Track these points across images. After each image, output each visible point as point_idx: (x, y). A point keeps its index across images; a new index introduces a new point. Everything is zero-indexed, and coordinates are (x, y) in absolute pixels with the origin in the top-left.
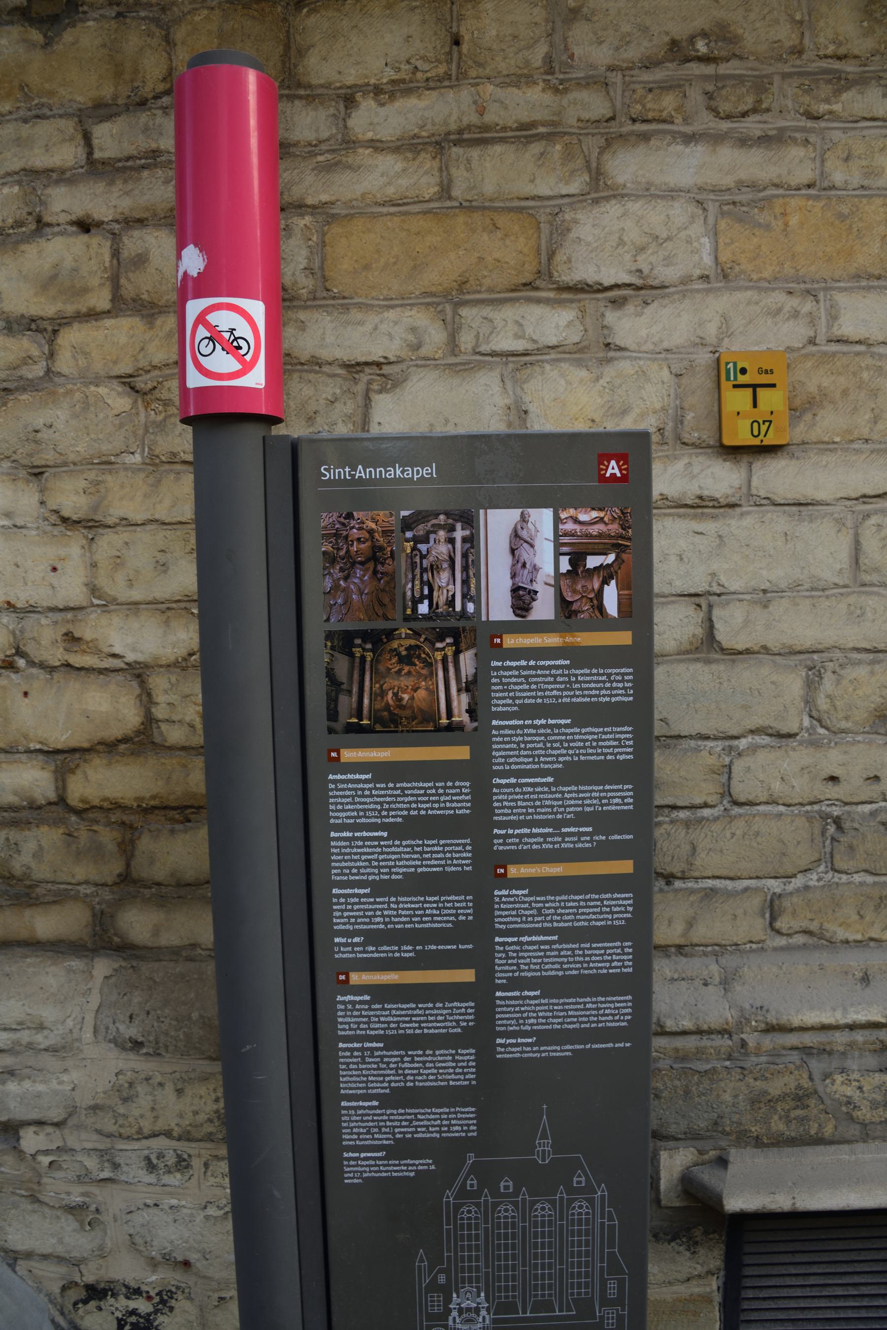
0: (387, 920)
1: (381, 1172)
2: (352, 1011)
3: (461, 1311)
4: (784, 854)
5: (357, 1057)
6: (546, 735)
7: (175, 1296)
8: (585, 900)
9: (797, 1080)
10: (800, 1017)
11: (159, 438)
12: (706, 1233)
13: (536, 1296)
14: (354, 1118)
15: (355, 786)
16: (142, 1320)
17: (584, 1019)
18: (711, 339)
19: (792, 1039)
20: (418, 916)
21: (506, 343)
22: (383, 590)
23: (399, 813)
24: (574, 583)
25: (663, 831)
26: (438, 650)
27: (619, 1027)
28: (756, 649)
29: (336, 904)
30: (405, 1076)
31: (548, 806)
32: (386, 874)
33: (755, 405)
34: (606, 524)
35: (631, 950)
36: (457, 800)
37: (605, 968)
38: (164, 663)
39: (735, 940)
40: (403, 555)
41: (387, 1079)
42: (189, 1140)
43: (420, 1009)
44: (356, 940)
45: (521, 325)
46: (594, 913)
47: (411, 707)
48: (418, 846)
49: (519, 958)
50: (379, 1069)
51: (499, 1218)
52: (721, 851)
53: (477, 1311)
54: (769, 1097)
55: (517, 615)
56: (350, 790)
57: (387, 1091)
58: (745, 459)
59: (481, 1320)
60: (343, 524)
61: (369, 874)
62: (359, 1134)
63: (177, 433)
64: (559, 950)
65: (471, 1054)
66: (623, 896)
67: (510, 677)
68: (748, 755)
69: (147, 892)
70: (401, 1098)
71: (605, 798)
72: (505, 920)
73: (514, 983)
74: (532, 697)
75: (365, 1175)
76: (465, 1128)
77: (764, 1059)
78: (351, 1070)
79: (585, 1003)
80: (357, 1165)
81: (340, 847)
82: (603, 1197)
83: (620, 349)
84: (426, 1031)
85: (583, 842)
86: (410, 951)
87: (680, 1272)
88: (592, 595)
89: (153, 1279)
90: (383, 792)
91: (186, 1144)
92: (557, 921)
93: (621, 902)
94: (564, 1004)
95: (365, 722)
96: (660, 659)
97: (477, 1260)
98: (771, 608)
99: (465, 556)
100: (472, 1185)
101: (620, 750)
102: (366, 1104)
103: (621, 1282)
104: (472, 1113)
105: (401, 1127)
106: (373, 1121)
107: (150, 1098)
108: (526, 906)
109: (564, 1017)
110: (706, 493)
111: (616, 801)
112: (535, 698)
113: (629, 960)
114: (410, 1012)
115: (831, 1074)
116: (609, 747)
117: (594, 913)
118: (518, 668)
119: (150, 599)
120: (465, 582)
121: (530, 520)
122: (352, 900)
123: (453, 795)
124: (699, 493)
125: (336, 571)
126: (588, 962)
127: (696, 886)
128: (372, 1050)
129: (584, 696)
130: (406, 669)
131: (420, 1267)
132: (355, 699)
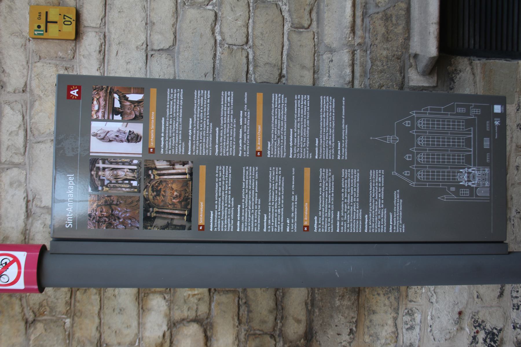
0: (279, 207)
1: (399, 215)
2: (322, 225)
3: (469, 181)
4: (272, 21)
5: (344, 224)
6: (197, 130)
7: (476, 319)
8: (275, 116)
9: (378, 20)
10: (348, 17)
11: (58, 310)
12: (451, 65)
13: (463, 146)
14: (373, 226)
15: (216, 219)
16: (489, 336)
17: (330, 118)
18: (23, 41)
19: (359, 21)
20: (278, 193)
21: (20, 140)
22: (125, 202)
23: (229, 199)
24: (126, 113)
25: (258, 78)
26: (154, 178)
27: (335, 102)
28: (174, 30)
29: (271, 230)
30: (354, 202)
31: (230, 131)
32: (258, 206)
33: (56, 22)
34: (100, 97)
35: (299, 96)
36: (224, 172)
37: (307, 108)
38: (168, 312)
39: (312, 46)
40: (109, 191)
41: (355, 210)
42: (398, 309)
43: (322, 193)
44: (288, 222)
45: (12, 132)
46: (281, 112)
47: (180, 191)
48: (245, 191)
49: (300, 147)
50: (350, 214)
51: (424, 161)
52: (270, 51)
53: (469, 173)
54: (386, 33)
55: (140, 140)
56: (218, 221)
57: (361, 210)
58: (82, 29)
59: (473, 172)
60: (94, 218)
61: (257, 215)
62: (381, 225)
63: (56, 301)
64: (297, 129)
65: (345, 171)
66: (273, 98)
67: (168, 145)
68: (224, 36)
69: (279, 325)
70: (364, 203)
71: (227, 104)
72: (282, 153)
73: (312, 149)
74: (179, 135)
75: (401, 222)
76: (380, 175)
77: (367, 35)
78: (350, 227)
79: (323, 118)
80: (396, 226)
81: (244, 227)
82: (416, 113)
83: (26, 85)
84: (333, 192)
85: (247, 116)
86: (295, 197)
87: (469, 78)
88: (133, 106)
89: (468, 330)
90: (219, 206)
91: (400, 310)
92: (284, 129)
93: (276, 99)
94: (323, 128)
95: (186, 213)
96: (177, 75)
97: (444, 172)
98: (155, 21)
99: (111, 163)
100: (408, 173)
101: (205, 96)
102: (366, 220)
103: (458, 106)
104: (372, 172)
105: (378, 205)
106: (375, 218)
107: (377, 327)
108: (276, 143)
109: (329, 128)
110: (98, 49)
111: (229, 99)
112: (179, 134)
113: (304, 97)
114: (323, 199)
115: (376, 3)
116: (204, 101)
117: (281, 112)
118: (165, 141)
119: (137, 317)
120: (124, 163)
121: (96, 132)
122: (269, 222)
123: (222, 174)
124: (98, 52)
125: (116, 223)
126: (304, 115)
127: (286, 64)
128: (341, 216)
129: (179, 112)
130: (162, 192)
131: (447, 199)
132: (175, 217)
